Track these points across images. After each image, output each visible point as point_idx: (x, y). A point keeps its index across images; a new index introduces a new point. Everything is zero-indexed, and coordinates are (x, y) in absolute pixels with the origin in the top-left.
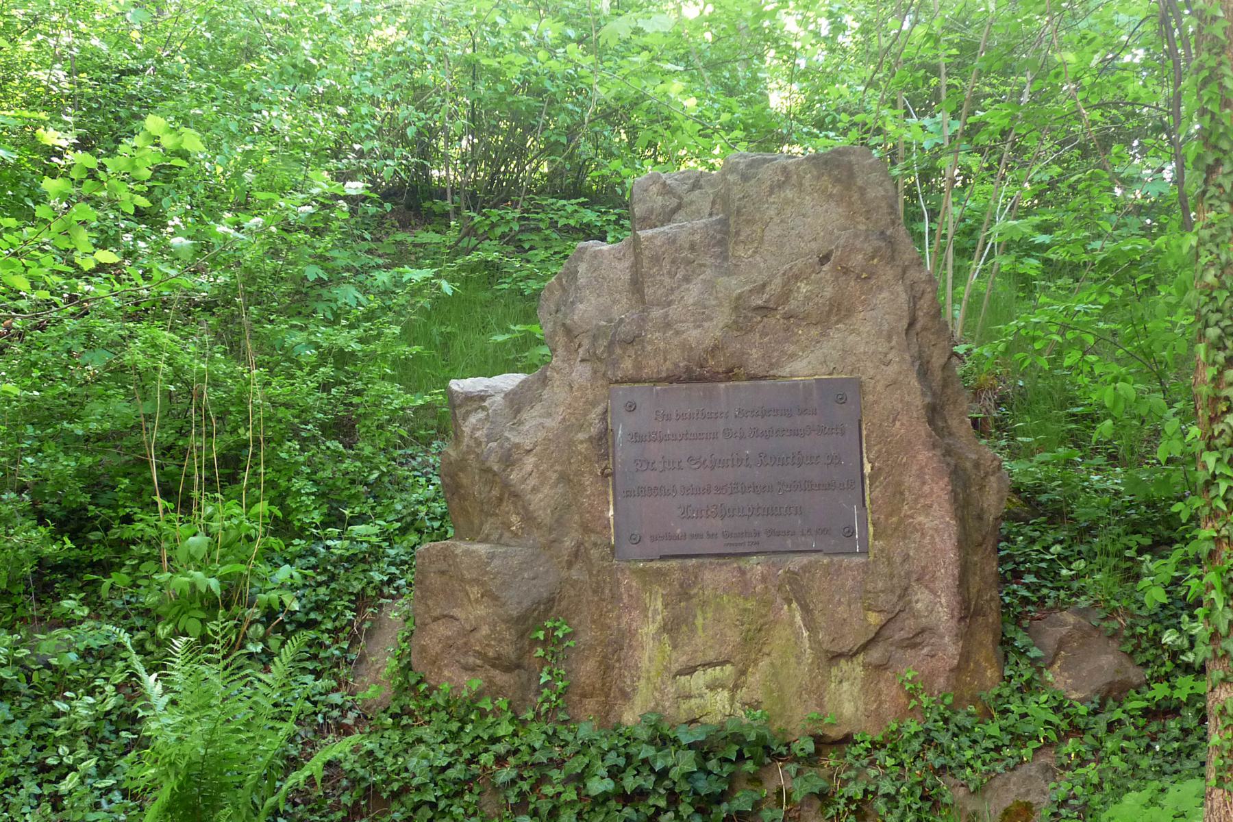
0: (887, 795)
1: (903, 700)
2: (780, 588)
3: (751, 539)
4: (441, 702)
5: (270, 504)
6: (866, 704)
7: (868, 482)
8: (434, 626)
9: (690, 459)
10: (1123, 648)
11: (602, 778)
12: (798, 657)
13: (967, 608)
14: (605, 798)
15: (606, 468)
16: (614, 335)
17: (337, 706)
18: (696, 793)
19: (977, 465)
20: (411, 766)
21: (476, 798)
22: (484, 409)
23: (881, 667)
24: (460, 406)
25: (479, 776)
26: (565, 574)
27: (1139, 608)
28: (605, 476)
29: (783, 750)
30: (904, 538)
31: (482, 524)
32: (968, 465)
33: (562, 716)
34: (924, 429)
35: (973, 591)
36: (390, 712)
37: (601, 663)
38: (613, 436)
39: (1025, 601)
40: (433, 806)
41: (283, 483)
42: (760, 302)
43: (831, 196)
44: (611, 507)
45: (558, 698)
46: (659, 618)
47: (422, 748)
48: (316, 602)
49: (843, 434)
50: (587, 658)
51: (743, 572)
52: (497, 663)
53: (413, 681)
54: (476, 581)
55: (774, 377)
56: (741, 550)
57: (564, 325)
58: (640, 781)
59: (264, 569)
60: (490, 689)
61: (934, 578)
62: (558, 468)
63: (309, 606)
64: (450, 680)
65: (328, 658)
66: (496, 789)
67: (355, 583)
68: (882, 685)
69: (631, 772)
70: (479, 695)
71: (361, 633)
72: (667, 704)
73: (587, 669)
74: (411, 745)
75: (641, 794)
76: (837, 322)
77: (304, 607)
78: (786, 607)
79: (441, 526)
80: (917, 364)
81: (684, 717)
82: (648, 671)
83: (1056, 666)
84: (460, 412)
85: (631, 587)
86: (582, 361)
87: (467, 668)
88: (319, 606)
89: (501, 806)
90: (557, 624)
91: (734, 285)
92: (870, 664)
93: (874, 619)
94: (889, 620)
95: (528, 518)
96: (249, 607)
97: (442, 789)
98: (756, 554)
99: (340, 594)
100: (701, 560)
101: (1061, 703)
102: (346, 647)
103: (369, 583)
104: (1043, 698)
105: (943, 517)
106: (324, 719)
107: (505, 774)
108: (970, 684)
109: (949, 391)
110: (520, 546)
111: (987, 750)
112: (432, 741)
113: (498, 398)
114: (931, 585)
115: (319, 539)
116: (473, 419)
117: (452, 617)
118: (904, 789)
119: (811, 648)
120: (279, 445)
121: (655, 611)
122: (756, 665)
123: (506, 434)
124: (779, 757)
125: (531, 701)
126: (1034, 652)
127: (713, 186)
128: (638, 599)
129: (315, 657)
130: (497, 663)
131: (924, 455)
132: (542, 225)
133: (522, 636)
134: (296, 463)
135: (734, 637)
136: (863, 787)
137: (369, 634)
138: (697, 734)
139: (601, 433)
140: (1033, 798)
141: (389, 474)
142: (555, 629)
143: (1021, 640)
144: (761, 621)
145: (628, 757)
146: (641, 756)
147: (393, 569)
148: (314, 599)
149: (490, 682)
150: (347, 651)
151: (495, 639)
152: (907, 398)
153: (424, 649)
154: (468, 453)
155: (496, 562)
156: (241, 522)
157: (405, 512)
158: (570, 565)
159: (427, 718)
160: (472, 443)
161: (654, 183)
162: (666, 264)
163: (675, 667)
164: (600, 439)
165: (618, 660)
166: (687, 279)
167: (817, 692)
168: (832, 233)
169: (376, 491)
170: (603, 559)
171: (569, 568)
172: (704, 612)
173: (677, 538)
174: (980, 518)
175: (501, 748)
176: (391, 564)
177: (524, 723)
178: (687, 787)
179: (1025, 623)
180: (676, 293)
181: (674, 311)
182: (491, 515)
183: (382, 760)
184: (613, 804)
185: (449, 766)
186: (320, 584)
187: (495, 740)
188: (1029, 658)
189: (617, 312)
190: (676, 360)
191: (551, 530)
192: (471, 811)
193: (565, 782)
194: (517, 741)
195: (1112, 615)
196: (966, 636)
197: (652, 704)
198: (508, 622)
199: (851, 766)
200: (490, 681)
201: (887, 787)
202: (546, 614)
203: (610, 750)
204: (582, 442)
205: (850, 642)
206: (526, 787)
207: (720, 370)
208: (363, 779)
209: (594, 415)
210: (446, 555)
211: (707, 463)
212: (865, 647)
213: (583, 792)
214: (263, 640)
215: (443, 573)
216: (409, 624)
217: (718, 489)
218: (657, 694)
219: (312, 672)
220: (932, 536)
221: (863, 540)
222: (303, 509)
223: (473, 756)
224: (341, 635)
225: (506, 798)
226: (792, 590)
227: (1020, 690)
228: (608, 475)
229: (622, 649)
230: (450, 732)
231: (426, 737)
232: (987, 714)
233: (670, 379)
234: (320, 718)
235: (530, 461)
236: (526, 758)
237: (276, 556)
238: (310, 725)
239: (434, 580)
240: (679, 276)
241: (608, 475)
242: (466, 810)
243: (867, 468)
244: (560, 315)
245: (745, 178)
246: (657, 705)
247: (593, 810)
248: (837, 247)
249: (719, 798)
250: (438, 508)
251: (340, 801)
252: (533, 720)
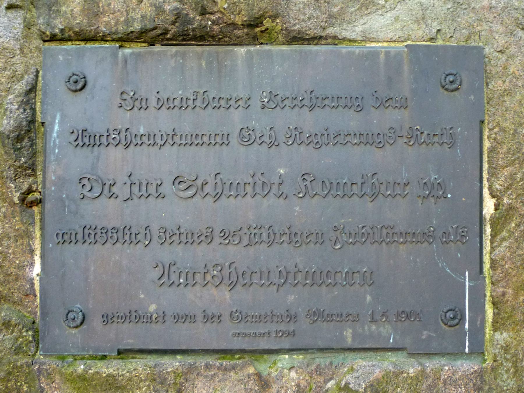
3: (282, 327)
7: (488, 230)
9: (177, 180)
49: (452, 145)
55: (335, 40)
56: (263, 344)
98: (290, 351)
100: (190, 360)
139: (19, 127)
164: (19, 139)
170: (18, 350)
207: (238, 20)
211: (208, 189)
217: (225, 235)
228: (32, 204)
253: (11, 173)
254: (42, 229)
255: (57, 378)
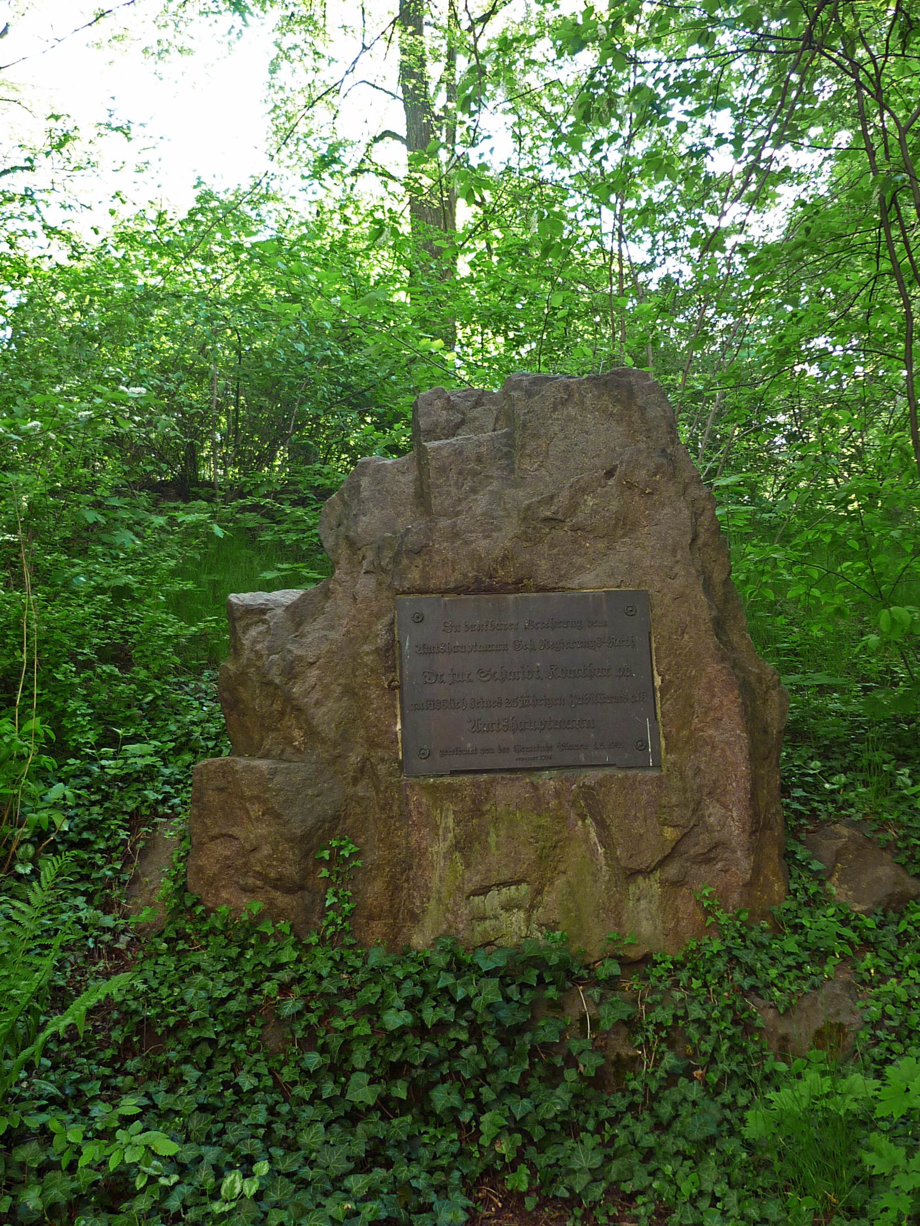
0: (698, 1021)
1: (700, 917)
2: (574, 804)
3: (544, 753)
4: (218, 925)
5: (42, 723)
6: (664, 922)
8: (211, 846)
9: (480, 671)
10: (897, 860)
11: (399, 1010)
12: (594, 875)
13: (758, 822)
14: (403, 1031)
15: (393, 681)
16: (400, 545)
17: (109, 929)
18: (499, 1023)
19: (760, 680)
20: (188, 997)
21: (259, 1031)
22: (264, 622)
23: (677, 884)
24: (240, 619)
25: (261, 1006)
26: (350, 790)
27: (910, 820)
28: (392, 689)
29: (585, 973)
30: (696, 751)
31: (262, 739)
32: (752, 679)
33: (348, 940)
34: (712, 641)
35: (762, 804)
36: (165, 936)
37: (389, 883)
38: (400, 648)
39: (799, 815)
40: (212, 1043)
41: (58, 704)
42: (548, 514)
43: (612, 415)
44: (399, 720)
45: (344, 921)
46: (450, 835)
47: (200, 977)
48: (89, 821)
49: (633, 646)
50: (374, 878)
51: (535, 788)
52: (279, 884)
53: (189, 903)
54: (257, 798)
55: (563, 589)
57: (347, 537)
58: (441, 1013)
59: (35, 788)
60: (273, 913)
61: (725, 792)
62: (342, 681)
63: (82, 825)
64: (228, 902)
65: (100, 879)
66: (280, 1021)
67: (128, 802)
68: (679, 902)
69: (429, 1003)
70: (260, 917)
71: (134, 853)
72: (461, 926)
73: (375, 889)
74: (188, 974)
75: (441, 1026)
76: (622, 537)
77: (77, 826)
78: (580, 823)
79: (216, 745)
80: (702, 578)
81: (478, 940)
82: (439, 892)
83: (834, 879)
84: (239, 625)
85: (420, 804)
86: (366, 572)
87: (245, 889)
88: (92, 826)
89: (286, 1041)
90: (343, 843)
91: (523, 496)
92: (667, 881)
93: (670, 833)
94: (685, 835)
95: (311, 733)
96: (19, 827)
97: (222, 1023)
99: (113, 813)
100: (492, 776)
101: (847, 915)
102: (119, 867)
103: (143, 802)
104: (831, 911)
105: (733, 730)
106: (95, 943)
107: (290, 1006)
108: (760, 898)
109: (729, 606)
110: (302, 761)
111: (789, 968)
112: (211, 969)
113: (279, 611)
114: (723, 799)
115: (93, 759)
116: (253, 632)
117: (231, 836)
118: (716, 1014)
119: (607, 865)
120: (57, 668)
121: (446, 829)
122: (552, 884)
123: (288, 646)
124: (579, 981)
125: (315, 924)
126: (816, 866)
127: (494, 404)
128: (428, 816)
129: (85, 878)
130: (279, 884)
131: (713, 668)
132: (301, 487)
133: (306, 856)
134: (72, 684)
135: (529, 854)
136: (672, 1012)
137: (144, 853)
138: (498, 960)
140: (845, 1019)
141: (161, 697)
142: (341, 848)
143: (801, 854)
144: (555, 838)
145: (424, 984)
146: (440, 985)
147: (168, 788)
148: (87, 818)
149: (271, 903)
150: (121, 871)
151: (277, 859)
152: (694, 611)
153: (200, 869)
154: (248, 666)
155: (278, 779)
156: (13, 740)
157: (179, 732)
158: (355, 781)
159: (204, 943)
160: (253, 656)
161: (439, 397)
162: (453, 475)
163: (469, 887)
164: (387, 650)
165: (407, 880)
166: (474, 490)
167: (615, 911)
168: (613, 450)
169: (152, 712)
170: (390, 774)
171: (354, 785)
172: (497, 829)
173: (468, 753)
174: (765, 731)
175: (284, 976)
176: (165, 783)
177: (308, 947)
178: (489, 1018)
179: (803, 836)
180: (464, 504)
181: (463, 521)
182: (272, 730)
183: (156, 990)
184: (409, 1038)
185: (231, 997)
186: (93, 804)
187: (278, 967)
188: (811, 871)
189: (401, 525)
190: (466, 570)
191: (335, 745)
192: (253, 1046)
193: (356, 1014)
194: (302, 968)
195: (883, 826)
196: (755, 850)
197: (444, 927)
198: (292, 841)
199: (654, 990)
200: (271, 904)
201: (696, 1012)
202: (330, 834)
203: (405, 978)
204: (368, 654)
205: (648, 858)
206: (314, 1020)
208: (136, 1012)
209: (380, 627)
210: (226, 771)
211: (497, 676)
212: (662, 864)
213: (377, 1025)
214: (33, 861)
215: (221, 790)
216: (184, 844)
218: (449, 916)
219: (84, 894)
220: (723, 750)
221: (656, 753)
222: (79, 730)
223: (256, 985)
224: (114, 855)
225: (293, 1032)
226: (587, 805)
227: (806, 904)
229: (410, 868)
230: (229, 958)
231: (204, 965)
232: (777, 930)
233: (457, 590)
234: (90, 943)
235: (313, 674)
236: (313, 988)
237: (50, 776)
238: (80, 950)
239: (212, 797)
240: (466, 487)
241: (396, 688)
242: (248, 1046)
243: (658, 681)
244: (342, 529)
245: (529, 394)
246: (450, 927)
247: (389, 1045)
248: (621, 462)
249: (519, 1029)
250: (212, 728)
251: (110, 1037)
252: (317, 945)
253: (382, 671)
254: (402, 702)
255: (417, 788)
